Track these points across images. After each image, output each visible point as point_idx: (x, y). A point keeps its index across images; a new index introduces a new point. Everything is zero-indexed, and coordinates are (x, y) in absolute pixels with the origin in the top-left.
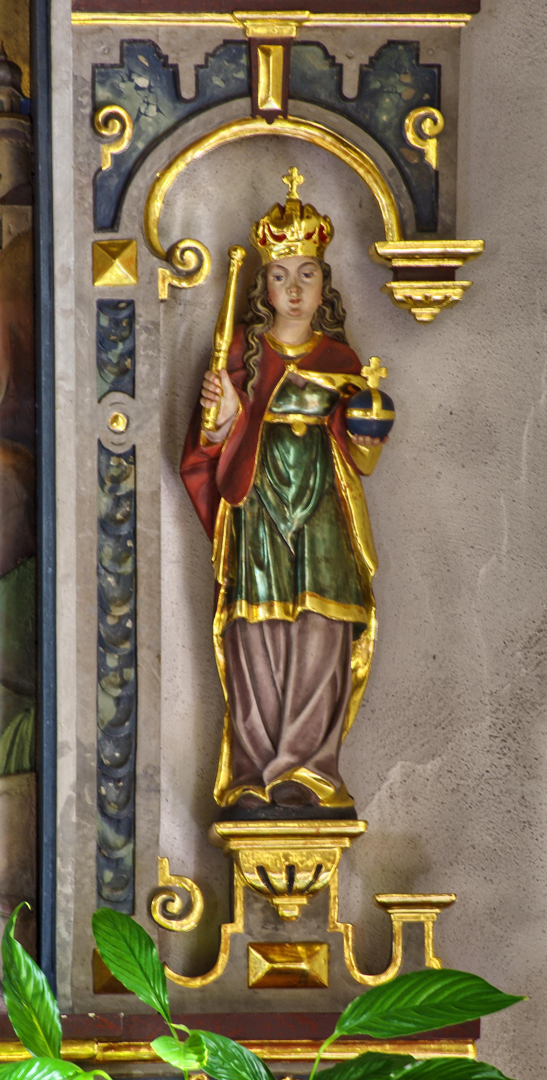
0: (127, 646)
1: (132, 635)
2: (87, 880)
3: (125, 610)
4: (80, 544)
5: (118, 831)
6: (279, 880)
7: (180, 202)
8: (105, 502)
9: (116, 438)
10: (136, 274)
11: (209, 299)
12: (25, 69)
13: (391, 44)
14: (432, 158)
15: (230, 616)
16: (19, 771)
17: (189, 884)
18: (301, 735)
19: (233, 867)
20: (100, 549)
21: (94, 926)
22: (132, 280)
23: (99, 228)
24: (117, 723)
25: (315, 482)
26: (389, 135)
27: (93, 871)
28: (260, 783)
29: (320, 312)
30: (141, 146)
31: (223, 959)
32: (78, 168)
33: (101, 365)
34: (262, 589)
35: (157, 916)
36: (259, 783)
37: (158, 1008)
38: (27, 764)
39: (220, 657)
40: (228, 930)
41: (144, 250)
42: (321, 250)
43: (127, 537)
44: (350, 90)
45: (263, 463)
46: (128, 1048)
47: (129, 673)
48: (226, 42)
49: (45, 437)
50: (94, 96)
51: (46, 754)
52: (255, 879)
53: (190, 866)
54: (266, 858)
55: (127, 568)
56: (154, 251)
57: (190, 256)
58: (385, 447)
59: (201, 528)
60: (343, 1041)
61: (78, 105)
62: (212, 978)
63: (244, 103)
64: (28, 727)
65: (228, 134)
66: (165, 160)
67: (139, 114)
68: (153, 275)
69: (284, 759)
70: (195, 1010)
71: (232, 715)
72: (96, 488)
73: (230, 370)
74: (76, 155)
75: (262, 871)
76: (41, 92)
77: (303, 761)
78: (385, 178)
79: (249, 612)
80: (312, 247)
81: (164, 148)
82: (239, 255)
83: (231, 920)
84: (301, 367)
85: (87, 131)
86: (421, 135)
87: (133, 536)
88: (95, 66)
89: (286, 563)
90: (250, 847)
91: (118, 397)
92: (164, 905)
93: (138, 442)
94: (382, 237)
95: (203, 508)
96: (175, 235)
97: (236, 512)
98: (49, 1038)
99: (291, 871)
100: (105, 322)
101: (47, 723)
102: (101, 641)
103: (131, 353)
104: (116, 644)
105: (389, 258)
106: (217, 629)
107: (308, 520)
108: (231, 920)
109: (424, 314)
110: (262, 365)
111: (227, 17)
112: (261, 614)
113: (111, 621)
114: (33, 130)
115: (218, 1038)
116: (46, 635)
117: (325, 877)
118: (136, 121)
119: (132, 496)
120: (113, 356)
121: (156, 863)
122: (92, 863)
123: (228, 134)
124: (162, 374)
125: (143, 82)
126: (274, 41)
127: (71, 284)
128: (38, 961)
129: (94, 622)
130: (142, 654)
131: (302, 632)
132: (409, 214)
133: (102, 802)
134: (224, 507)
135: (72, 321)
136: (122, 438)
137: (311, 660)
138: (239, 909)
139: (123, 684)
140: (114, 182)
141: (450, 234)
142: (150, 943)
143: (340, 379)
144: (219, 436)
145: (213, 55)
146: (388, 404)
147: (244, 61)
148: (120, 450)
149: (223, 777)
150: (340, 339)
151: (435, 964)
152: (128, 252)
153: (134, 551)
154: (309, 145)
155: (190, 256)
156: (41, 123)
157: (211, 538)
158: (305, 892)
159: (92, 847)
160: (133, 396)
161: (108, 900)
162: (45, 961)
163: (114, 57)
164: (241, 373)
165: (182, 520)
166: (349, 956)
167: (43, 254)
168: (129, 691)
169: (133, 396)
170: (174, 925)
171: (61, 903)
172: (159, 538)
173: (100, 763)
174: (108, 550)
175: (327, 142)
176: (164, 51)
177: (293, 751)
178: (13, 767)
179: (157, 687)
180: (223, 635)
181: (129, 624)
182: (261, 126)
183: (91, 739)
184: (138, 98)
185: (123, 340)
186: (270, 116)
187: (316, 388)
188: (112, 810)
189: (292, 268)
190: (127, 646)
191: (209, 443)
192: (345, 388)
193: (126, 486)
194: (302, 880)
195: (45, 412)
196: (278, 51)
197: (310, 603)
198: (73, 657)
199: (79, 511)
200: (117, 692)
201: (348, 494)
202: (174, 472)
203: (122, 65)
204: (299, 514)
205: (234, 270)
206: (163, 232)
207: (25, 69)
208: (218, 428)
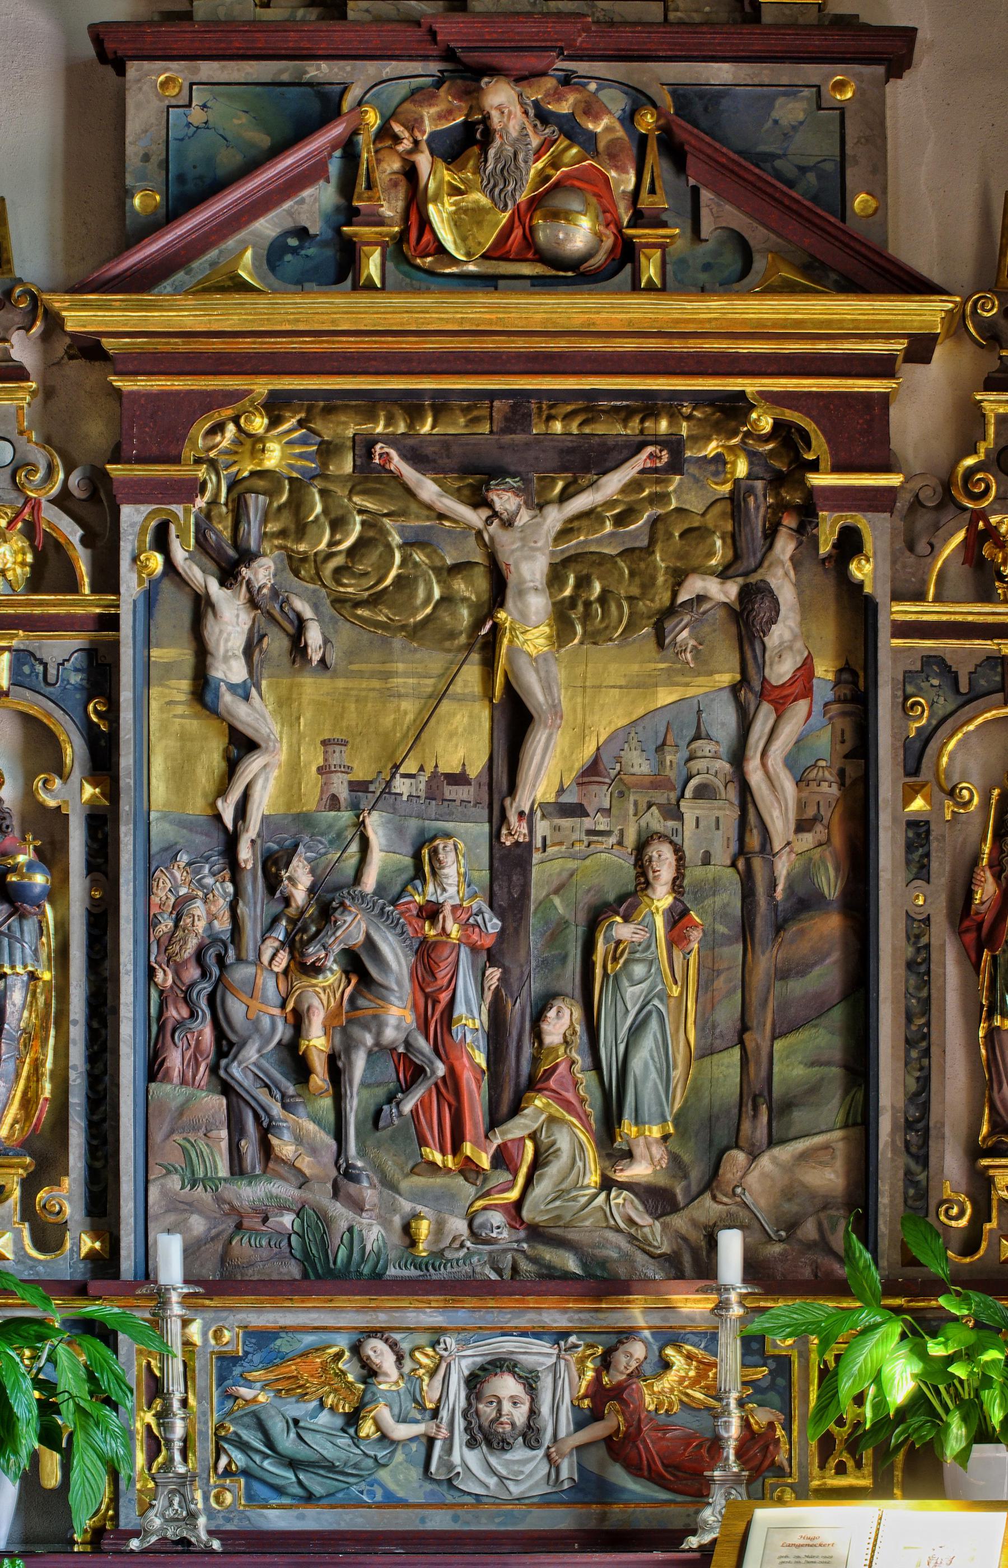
0: (924, 1044)
1: (926, 1037)
2: (898, 1195)
3: (923, 1021)
4: (894, 978)
5: (917, 1163)
7: (959, 759)
8: (911, 950)
9: (918, 910)
10: (930, 804)
11: (977, 820)
12: (861, 674)
15: (990, 1025)
17: (962, 1197)
20: (907, 981)
21: (902, 1224)
22: (928, 808)
23: (907, 774)
24: (917, 1094)
27: (902, 1189)
30: (934, 722)
31: (984, 1245)
33: (908, 862)
35: (942, 1218)
37: (943, 1276)
38: (859, 1120)
39: (983, 1051)
40: (988, 1226)
41: (936, 789)
43: (924, 974)
46: (923, 1301)
48: (988, 658)
49: (872, 908)
50: (904, 691)
51: (872, 1114)
53: (964, 1187)
55: (924, 994)
57: (965, 792)
59: (971, 968)
61: (894, 696)
64: (860, 1096)
65: (988, 715)
66: (949, 731)
67: (933, 703)
71: (991, 1089)
72: (904, 942)
73: (991, 866)
74: (893, 728)
76: (871, 689)
79: (1002, 1022)
81: (950, 722)
82: (996, 792)
83: (990, 1221)
85: (899, 712)
87: (928, 972)
88: (905, 672)
90: (777, 195)
91: (919, 883)
92: (947, 1210)
93: (931, 912)
95: (973, 955)
96: (956, 779)
97: (994, 958)
98: (873, 1295)
100: (911, 835)
101: (872, 1094)
102: (907, 1041)
103: (927, 855)
104: (917, 1042)
106: (981, 1034)
108: (990, 1221)
111: (989, 642)
113: (914, 1028)
114: (866, 712)
115: (981, 1295)
116: (872, 1036)
118: (931, 706)
119: (927, 946)
120: (916, 856)
121: (941, 1184)
122: (901, 1183)
123: (988, 715)
124: (947, 868)
125: (936, 682)
127: (889, 810)
128: (866, 1246)
129: (903, 1029)
130: (934, 1049)
133: (907, 1144)
134: (986, 955)
135: (890, 834)
136: (921, 910)
138: (994, 1213)
139: (921, 1069)
140: (918, 745)
142: (938, 1235)
145: (980, 665)
147: (999, 669)
148: (920, 917)
149: (985, 1129)
152: (926, 790)
153: (928, 983)
156: (871, 707)
157: (978, 974)
159: (901, 1173)
160: (928, 882)
161: (911, 1208)
162: (871, 1246)
163: (918, 666)
164: (998, 868)
165: (959, 962)
167: (872, 791)
168: (925, 1073)
169: (928, 882)
170: (953, 1224)
172: (945, 974)
173: (906, 1120)
174: (912, 982)
176: (949, 663)
178: (850, 1121)
179: (943, 1071)
180: (985, 1037)
181: (925, 1030)
183: (901, 1104)
184: (933, 693)
185: (922, 846)
188: (914, 1150)
190: (924, 1044)
191: (977, 913)
193: (924, 941)
195: (872, 892)
198: (889, 1051)
199: (894, 956)
200: (918, 1074)
202: (954, 932)
203: (922, 671)
205: (993, 801)
206: (948, 777)
207: (861, 674)
208: (982, 903)
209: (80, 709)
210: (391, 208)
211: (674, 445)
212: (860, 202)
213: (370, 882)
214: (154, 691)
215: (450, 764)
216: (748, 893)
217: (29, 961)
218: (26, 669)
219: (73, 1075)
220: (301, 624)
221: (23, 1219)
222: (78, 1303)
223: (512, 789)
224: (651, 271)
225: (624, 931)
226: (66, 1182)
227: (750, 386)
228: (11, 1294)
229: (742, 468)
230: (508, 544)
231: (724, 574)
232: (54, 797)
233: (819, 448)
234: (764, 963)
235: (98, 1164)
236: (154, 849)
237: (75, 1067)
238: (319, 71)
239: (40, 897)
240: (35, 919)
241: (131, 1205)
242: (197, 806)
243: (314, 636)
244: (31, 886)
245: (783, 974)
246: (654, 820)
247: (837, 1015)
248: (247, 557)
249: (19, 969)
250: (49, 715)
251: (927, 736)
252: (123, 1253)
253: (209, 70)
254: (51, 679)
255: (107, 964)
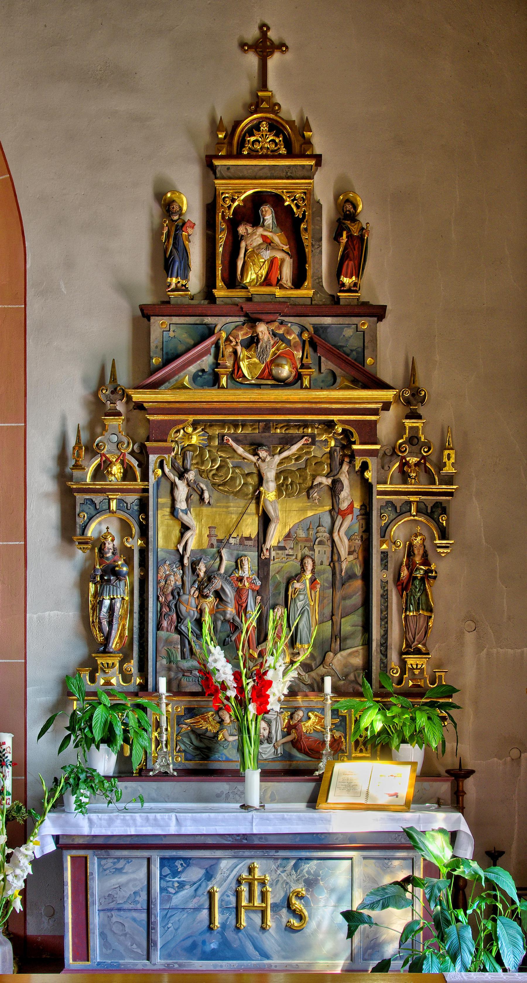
0: (386, 620)
1: (387, 618)
3: (386, 613)
4: (377, 600)
6: (415, 667)
11: (402, 552)
13: (437, 502)
14: (445, 524)
16: (365, 644)
17: (397, 667)
18: (419, 638)
19: (340, 260)
23: (381, 537)
24: (384, 635)
25: (422, 588)
26: (436, 520)
28: (411, 647)
29: (423, 554)
31: (404, 682)
32: (377, 526)
33: (381, 564)
34: (412, 609)
36: (411, 647)
40: (405, 676)
42: (423, 542)
44: (429, 511)
45: (412, 584)
47: (386, 625)
52: (410, 666)
54: (412, 662)
56: (392, 542)
57: (398, 543)
58: (436, 581)
60: (426, 698)
61: (377, 513)
62: (403, 684)
63: (409, 513)
64: (367, 636)
68: (391, 547)
69: (416, 643)
70: (398, 692)
73: (406, 565)
75: (411, 665)
77: (419, 644)
78: (436, 528)
80: (422, 541)
82: (408, 543)
84: (420, 565)
86: (443, 520)
89: (416, 604)
94: (435, 540)
97: (407, 594)
99: (417, 665)
102: (381, 619)
103: (387, 562)
105: (436, 544)
107: (421, 595)
109: (443, 555)
110: (412, 565)
112: (411, 614)
117: (423, 666)
118: (388, 517)
119: (387, 590)
120: (384, 562)
121: (391, 663)
125: (390, 509)
126: (415, 501)
130: (389, 622)
131: (419, 618)
132: (440, 535)
133: (381, 651)
134: (405, 593)
137: (421, 623)
138: (407, 672)
139: (385, 628)
140: (384, 528)
141: (448, 539)
142: (390, 679)
143: (427, 568)
144: (404, 578)
146: (436, 573)
149: (404, 646)
150: (427, 559)
151: (444, 683)
154: (421, 521)
155: (398, 543)
158: (419, 669)
159: (379, 659)
165: (396, 595)
166: (428, 681)
170: (395, 675)
171: (373, 670)
174: (382, 601)
175: (425, 521)
177: (417, 641)
182: (412, 518)
186: (414, 516)
187: (422, 569)
188: (383, 652)
189: (418, 546)
190: (386, 620)
192: (428, 569)
193: (386, 588)
194: (419, 666)
196: (415, 503)
197: (421, 612)
201: (428, 590)
204: (419, 594)
209: (137, 517)
210: (229, 363)
211: (313, 436)
212: (369, 361)
213: (222, 571)
214: (159, 512)
215: (246, 534)
216: (334, 574)
217: (122, 594)
218: (121, 505)
219: (135, 629)
220: (202, 491)
221: (119, 673)
222: (136, 699)
223: (264, 542)
224: (306, 382)
225: (297, 585)
226: (132, 661)
227: (335, 418)
228: (115, 696)
229: (333, 444)
230: (264, 467)
231: (327, 476)
232: (130, 544)
233: (356, 437)
234: (338, 595)
235: (142, 656)
236: (159, 560)
237: (135, 627)
238: (208, 320)
239: (125, 574)
240: (124, 581)
241: (152, 669)
242: (172, 547)
243: (206, 495)
244: (123, 571)
245: (344, 598)
246: (306, 551)
247: (360, 611)
248: (187, 471)
249: (119, 596)
250: (128, 519)
251: (387, 526)
252: (149, 683)
253: (175, 320)
254: (129, 508)
255: (145, 595)
